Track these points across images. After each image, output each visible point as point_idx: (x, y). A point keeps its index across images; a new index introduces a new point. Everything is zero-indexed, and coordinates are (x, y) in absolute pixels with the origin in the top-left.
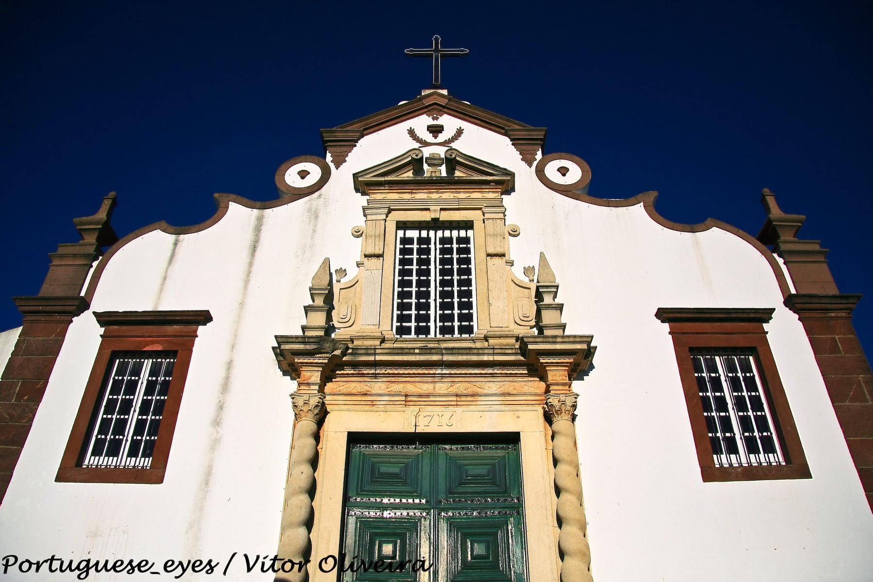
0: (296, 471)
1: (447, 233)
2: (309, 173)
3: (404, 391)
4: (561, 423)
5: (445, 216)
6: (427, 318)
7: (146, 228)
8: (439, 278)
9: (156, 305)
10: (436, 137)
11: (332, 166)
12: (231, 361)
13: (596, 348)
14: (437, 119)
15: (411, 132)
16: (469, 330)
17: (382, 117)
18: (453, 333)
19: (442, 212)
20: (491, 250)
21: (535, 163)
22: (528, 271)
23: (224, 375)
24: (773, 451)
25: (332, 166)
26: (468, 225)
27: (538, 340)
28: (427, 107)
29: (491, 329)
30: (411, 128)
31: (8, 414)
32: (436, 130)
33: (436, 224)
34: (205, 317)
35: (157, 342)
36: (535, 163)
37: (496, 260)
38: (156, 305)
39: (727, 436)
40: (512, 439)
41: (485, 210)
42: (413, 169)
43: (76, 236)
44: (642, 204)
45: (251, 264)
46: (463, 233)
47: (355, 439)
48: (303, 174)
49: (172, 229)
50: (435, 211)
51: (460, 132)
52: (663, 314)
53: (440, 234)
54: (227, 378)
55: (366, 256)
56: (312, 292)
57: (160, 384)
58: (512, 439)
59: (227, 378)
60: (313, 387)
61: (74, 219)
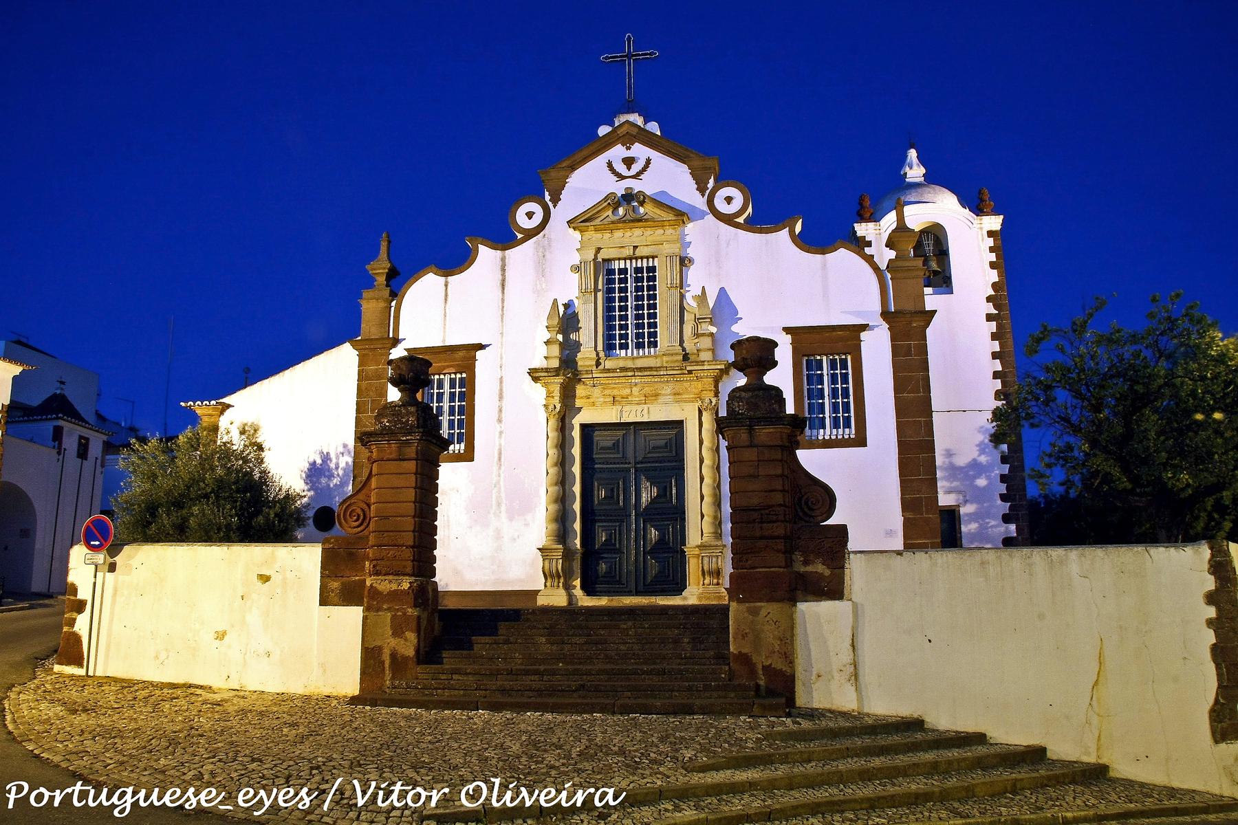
2: (534, 213)
3: (612, 394)
7: (421, 273)
9: (444, 341)
10: (629, 168)
11: (550, 204)
12: (502, 377)
13: (581, 328)
14: (629, 148)
15: (610, 165)
16: (655, 345)
17: (585, 153)
18: (833, 398)
21: (708, 192)
23: (499, 388)
24: (849, 426)
25: (550, 204)
30: (609, 161)
31: (369, 422)
32: (629, 162)
34: (481, 347)
35: (451, 366)
36: (708, 192)
38: (444, 341)
39: (1189, 538)
40: (679, 424)
42: (422, 402)
43: (369, 283)
45: (503, 300)
48: (530, 215)
49: (440, 272)
51: (648, 162)
54: (501, 390)
57: (611, 124)
58: (679, 424)
59: (501, 390)
61: (788, 412)
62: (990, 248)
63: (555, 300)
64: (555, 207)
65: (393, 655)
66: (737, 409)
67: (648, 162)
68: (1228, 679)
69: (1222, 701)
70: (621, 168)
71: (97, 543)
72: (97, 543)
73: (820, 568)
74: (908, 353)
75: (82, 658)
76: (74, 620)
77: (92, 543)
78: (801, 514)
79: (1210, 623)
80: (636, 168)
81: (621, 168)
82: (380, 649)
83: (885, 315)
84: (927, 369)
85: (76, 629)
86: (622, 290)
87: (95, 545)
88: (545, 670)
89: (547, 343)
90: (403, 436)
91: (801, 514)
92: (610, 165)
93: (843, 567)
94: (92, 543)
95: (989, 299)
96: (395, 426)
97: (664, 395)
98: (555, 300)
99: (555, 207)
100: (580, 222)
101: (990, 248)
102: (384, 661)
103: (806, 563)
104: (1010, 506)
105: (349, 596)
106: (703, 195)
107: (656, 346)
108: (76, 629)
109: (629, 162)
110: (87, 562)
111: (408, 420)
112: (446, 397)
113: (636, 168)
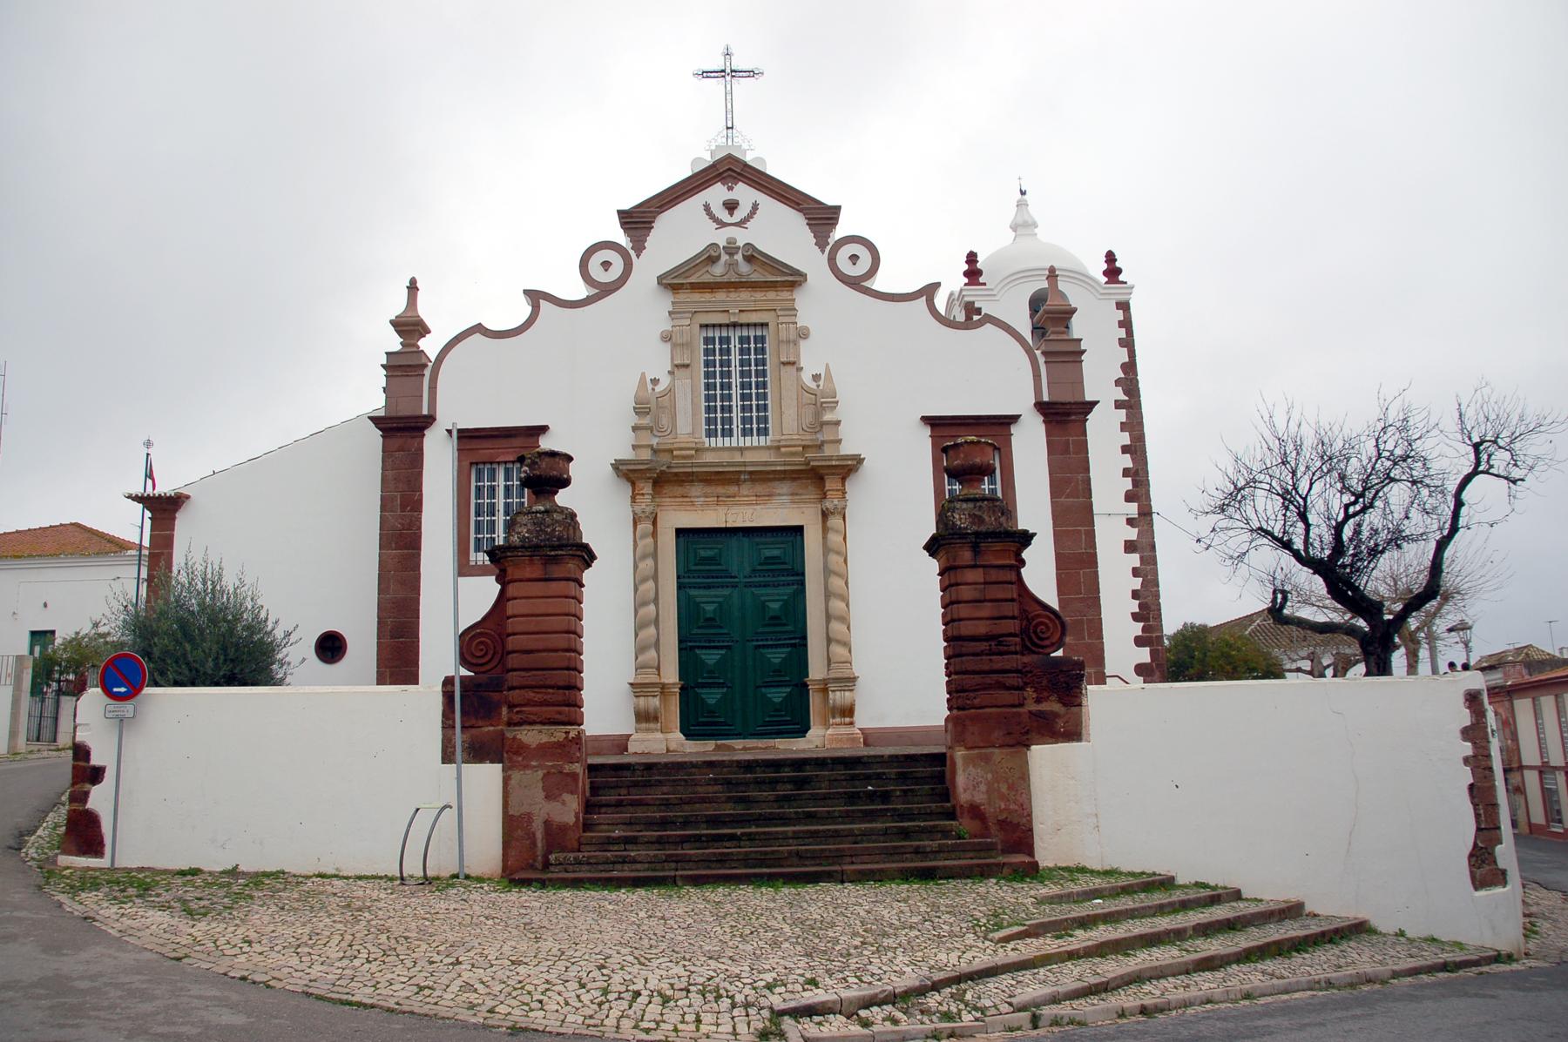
0: (642, 565)
1: (745, 333)
4: (834, 521)
5: (744, 319)
6: (729, 397)
8: (739, 380)
11: (632, 253)
15: (707, 208)
16: (763, 432)
19: (742, 314)
20: (784, 359)
21: (828, 248)
22: (816, 378)
25: (632, 253)
26: (764, 325)
27: (766, 598)
28: (720, 174)
29: (783, 437)
32: (731, 206)
33: (735, 325)
36: (828, 248)
37: (789, 368)
40: (799, 530)
41: (779, 313)
44: (924, 298)
46: (759, 333)
47: (680, 532)
50: (734, 314)
51: (755, 207)
52: (928, 420)
53: (738, 333)
55: (676, 366)
56: (682, 580)
58: (799, 530)
60: (646, 497)
62: (1119, 322)
63: (643, 374)
64: (638, 256)
65: (547, 823)
66: (958, 523)
67: (755, 207)
68: (1486, 821)
69: (1480, 845)
70: (723, 215)
71: (123, 690)
72: (123, 690)
73: (1052, 706)
74: (1066, 451)
75: (101, 844)
76: (87, 794)
77: (115, 690)
78: (1029, 645)
79: (1466, 761)
80: (740, 214)
81: (723, 215)
82: (528, 817)
83: (1041, 406)
84: (1087, 470)
85: (90, 805)
86: (759, 374)
87: (119, 692)
88: (742, 834)
89: (635, 429)
90: (550, 551)
91: (1029, 645)
92: (707, 208)
93: (1080, 705)
94: (115, 690)
95: (1118, 382)
96: (537, 537)
97: (779, 495)
98: (643, 374)
99: (638, 256)
100: (673, 283)
101: (1119, 322)
102: (534, 834)
103: (1038, 701)
104: (1144, 627)
105: (479, 752)
106: (823, 252)
107: (766, 434)
108: (90, 805)
109: (731, 206)
110: (111, 715)
111: (554, 530)
112: (501, 492)
113: (740, 214)
